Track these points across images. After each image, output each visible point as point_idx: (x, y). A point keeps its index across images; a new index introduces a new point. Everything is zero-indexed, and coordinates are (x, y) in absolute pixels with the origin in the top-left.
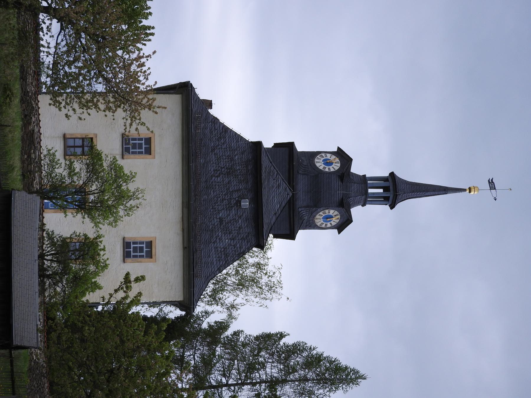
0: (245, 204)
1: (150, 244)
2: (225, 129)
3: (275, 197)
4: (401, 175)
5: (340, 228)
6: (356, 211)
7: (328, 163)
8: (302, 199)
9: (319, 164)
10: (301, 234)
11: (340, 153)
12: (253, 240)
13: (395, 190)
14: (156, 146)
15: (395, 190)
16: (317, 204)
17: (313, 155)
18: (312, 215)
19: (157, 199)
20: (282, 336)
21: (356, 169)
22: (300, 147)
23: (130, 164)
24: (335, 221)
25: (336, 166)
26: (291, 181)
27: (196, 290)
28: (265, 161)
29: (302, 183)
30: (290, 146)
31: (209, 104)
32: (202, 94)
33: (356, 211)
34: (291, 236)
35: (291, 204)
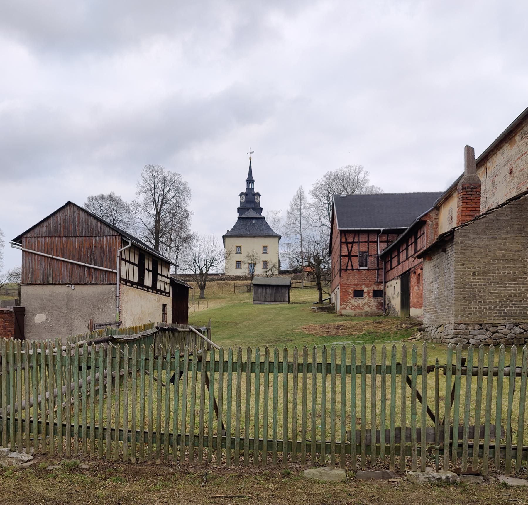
0: (254, 222)
1: (264, 247)
2: (234, 226)
3: (252, 214)
4: (246, 179)
5: (260, 195)
6: (256, 191)
7: (243, 199)
8: (252, 206)
9: (243, 201)
10: (261, 206)
11: (240, 195)
12: (304, 298)
13: (250, 180)
14: (238, 245)
15: (250, 180)
16: (253, 202)
17: (241, 203)
18: (256, 203)
19: (251, 246)
20: (300, 196)
21: (244, 191)
22: (239, 206)
23: (121, 327)
24: (258, 197)
25: (244, 196)
26: (249, 209)
27: (274, 235)
28: (243, 216)
29: (248, 206)
30: (238, 209)
31: (228, 231)
32: (225, 233)
33: (256, 191)
34: (262, 209)
35: (253, 209)
